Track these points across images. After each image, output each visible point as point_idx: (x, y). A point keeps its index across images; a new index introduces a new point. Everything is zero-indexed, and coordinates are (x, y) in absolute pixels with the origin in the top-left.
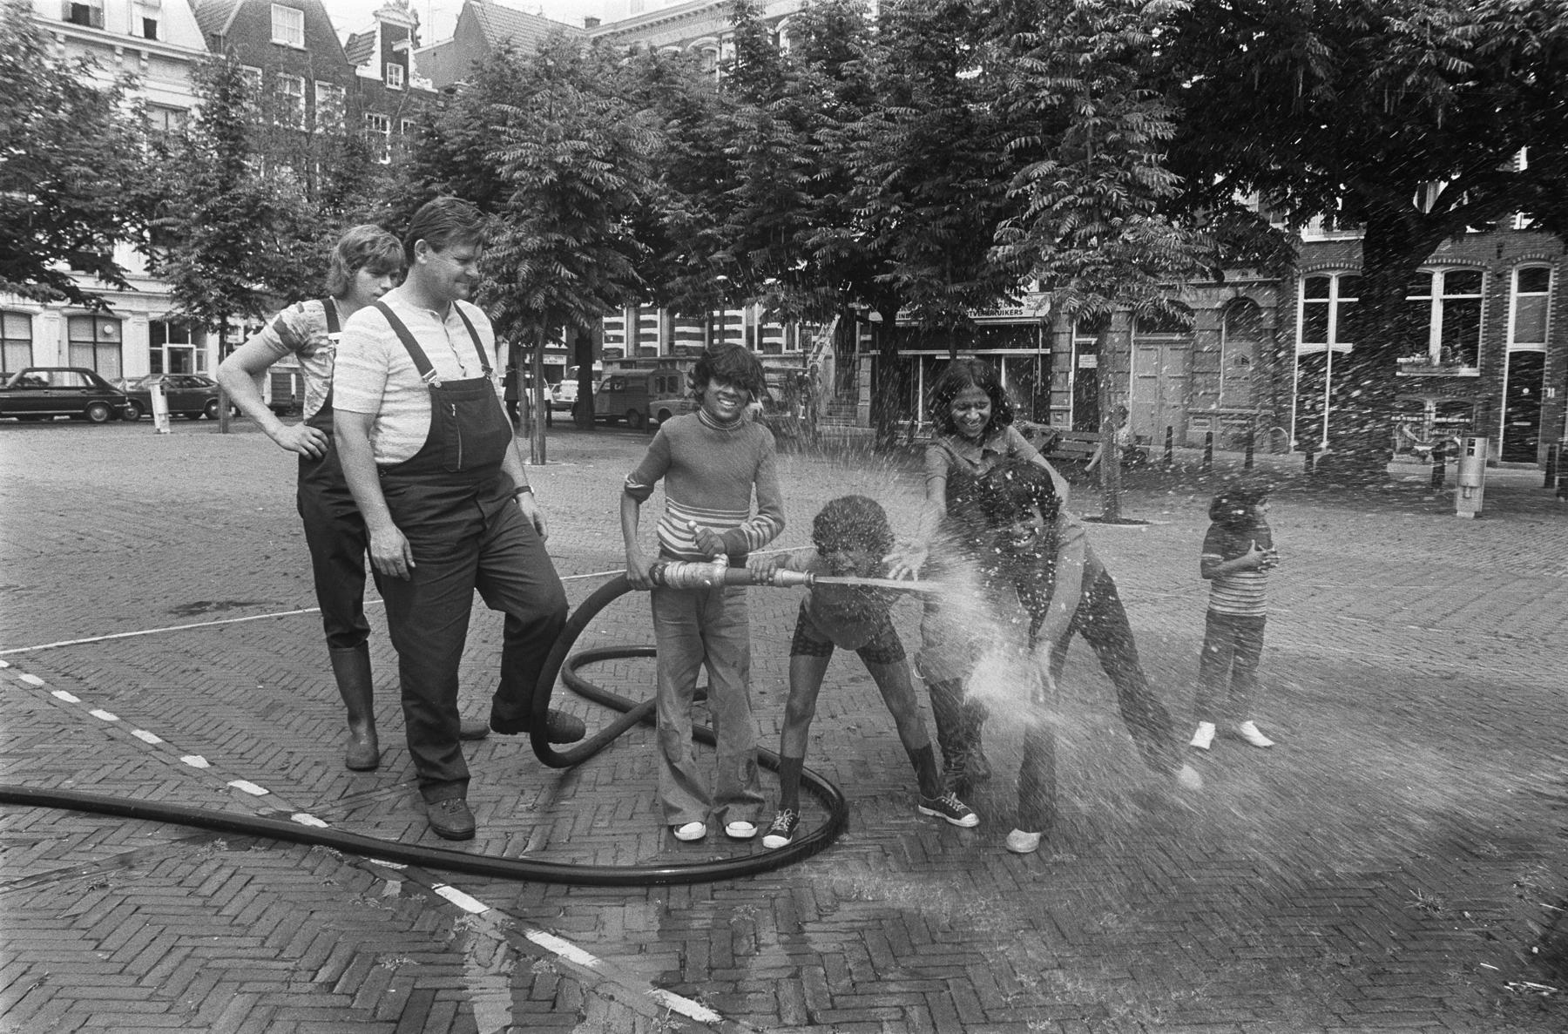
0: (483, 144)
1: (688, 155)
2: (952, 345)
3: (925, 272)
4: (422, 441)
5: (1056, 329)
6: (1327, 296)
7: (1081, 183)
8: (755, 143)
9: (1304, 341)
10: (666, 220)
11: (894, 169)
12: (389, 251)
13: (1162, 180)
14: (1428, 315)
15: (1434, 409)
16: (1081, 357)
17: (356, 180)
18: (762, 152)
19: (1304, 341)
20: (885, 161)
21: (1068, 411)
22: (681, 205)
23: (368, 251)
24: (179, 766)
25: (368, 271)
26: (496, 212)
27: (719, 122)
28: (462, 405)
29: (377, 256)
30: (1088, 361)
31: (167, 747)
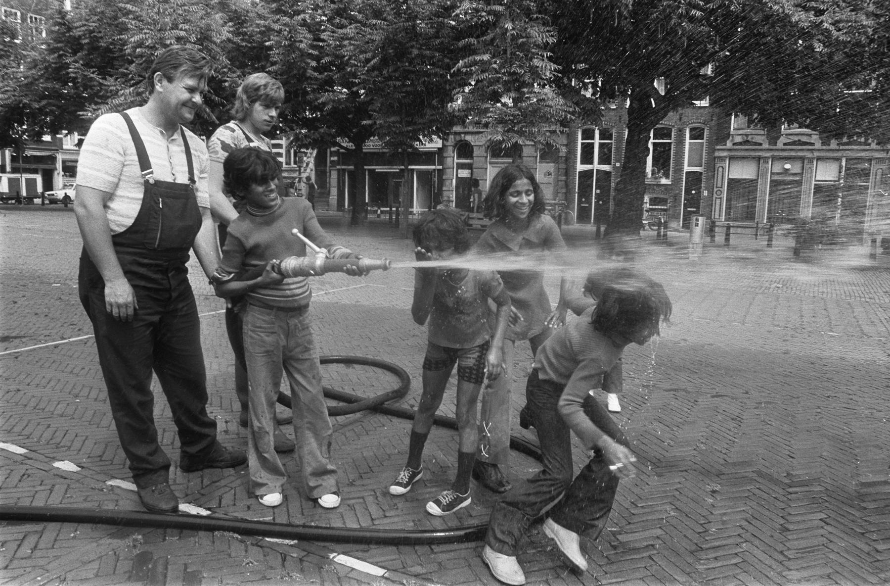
0: (100, 32)
1: (238, 45)
2: (406, 163)
3: (392, 119)
4: (130, 222)
5: (445, 155)
6: (593, 139)
7: (504, 67)
8: (286, 39)
9: (582, 163)
10: (227, 84)
11: (373, 58)
12: (275, 92)
13: (548, 69)
14: (593, 148)
15: (648, 201)
16: (459, 171)
17: (6, 51)
18: (289, 45)
19: (582, 163)
20: (366, 53)
21: (452, 201)
22: (235, 75)
23: (262, 92)
24: (54, 472)
25: (261, 105)
26: (111, 76)
27: (258, 26)
28: (167, 200)
29: (268, 95)
30: (464, 173)
31: (32, 455)
